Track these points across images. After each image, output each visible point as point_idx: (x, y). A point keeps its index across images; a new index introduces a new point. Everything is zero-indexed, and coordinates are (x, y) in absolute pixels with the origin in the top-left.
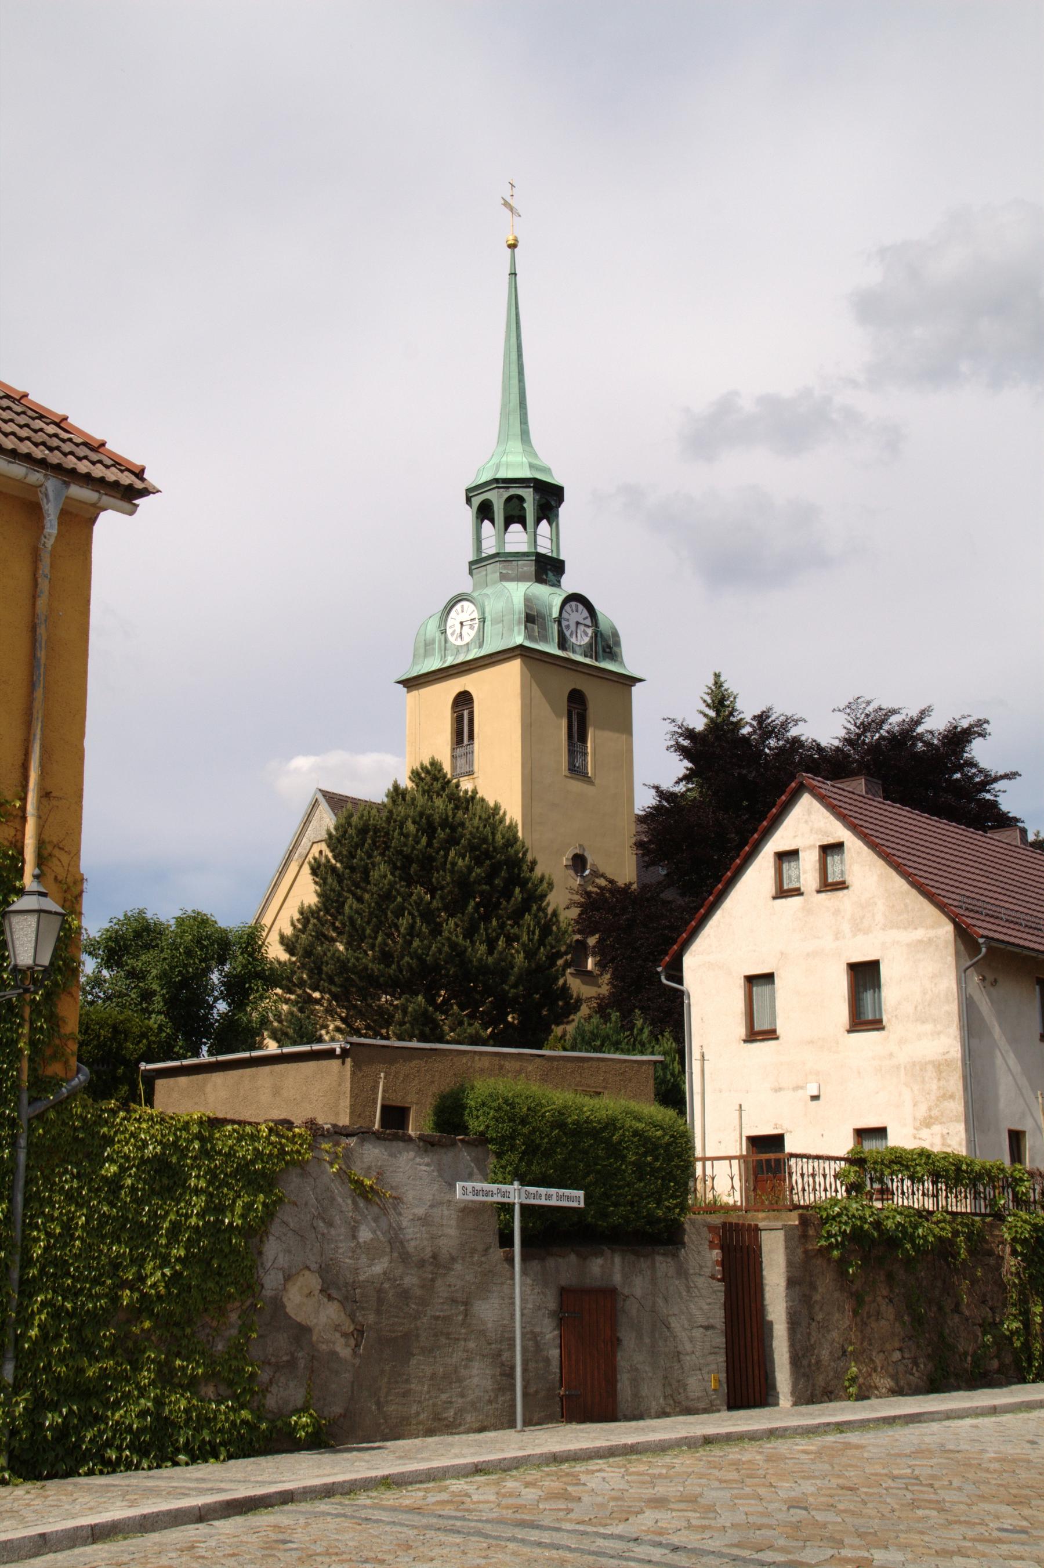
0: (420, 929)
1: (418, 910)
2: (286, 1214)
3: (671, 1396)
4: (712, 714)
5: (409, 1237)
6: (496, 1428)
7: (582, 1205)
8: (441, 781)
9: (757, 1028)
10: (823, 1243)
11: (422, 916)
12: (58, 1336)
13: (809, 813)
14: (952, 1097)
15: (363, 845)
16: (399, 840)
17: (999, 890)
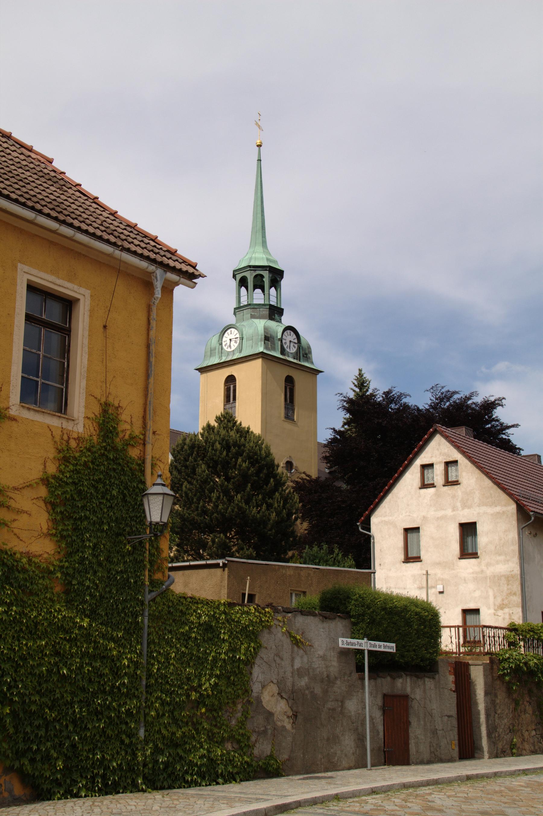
0: (223, 499)
1: (222, 490)
2: (263, 653)
3: (434, 752)
4: (357, 390)
5: (316, 666)
6: (356, 768)
7: (395, 651)
8: (232, 422)
9: (410, 556)
10: (501, 673)
12: (164, 715)
13: (439, 445)
14: (515, 594)
15: (192, 455)
16: (212, 452)
17: (534, 487)
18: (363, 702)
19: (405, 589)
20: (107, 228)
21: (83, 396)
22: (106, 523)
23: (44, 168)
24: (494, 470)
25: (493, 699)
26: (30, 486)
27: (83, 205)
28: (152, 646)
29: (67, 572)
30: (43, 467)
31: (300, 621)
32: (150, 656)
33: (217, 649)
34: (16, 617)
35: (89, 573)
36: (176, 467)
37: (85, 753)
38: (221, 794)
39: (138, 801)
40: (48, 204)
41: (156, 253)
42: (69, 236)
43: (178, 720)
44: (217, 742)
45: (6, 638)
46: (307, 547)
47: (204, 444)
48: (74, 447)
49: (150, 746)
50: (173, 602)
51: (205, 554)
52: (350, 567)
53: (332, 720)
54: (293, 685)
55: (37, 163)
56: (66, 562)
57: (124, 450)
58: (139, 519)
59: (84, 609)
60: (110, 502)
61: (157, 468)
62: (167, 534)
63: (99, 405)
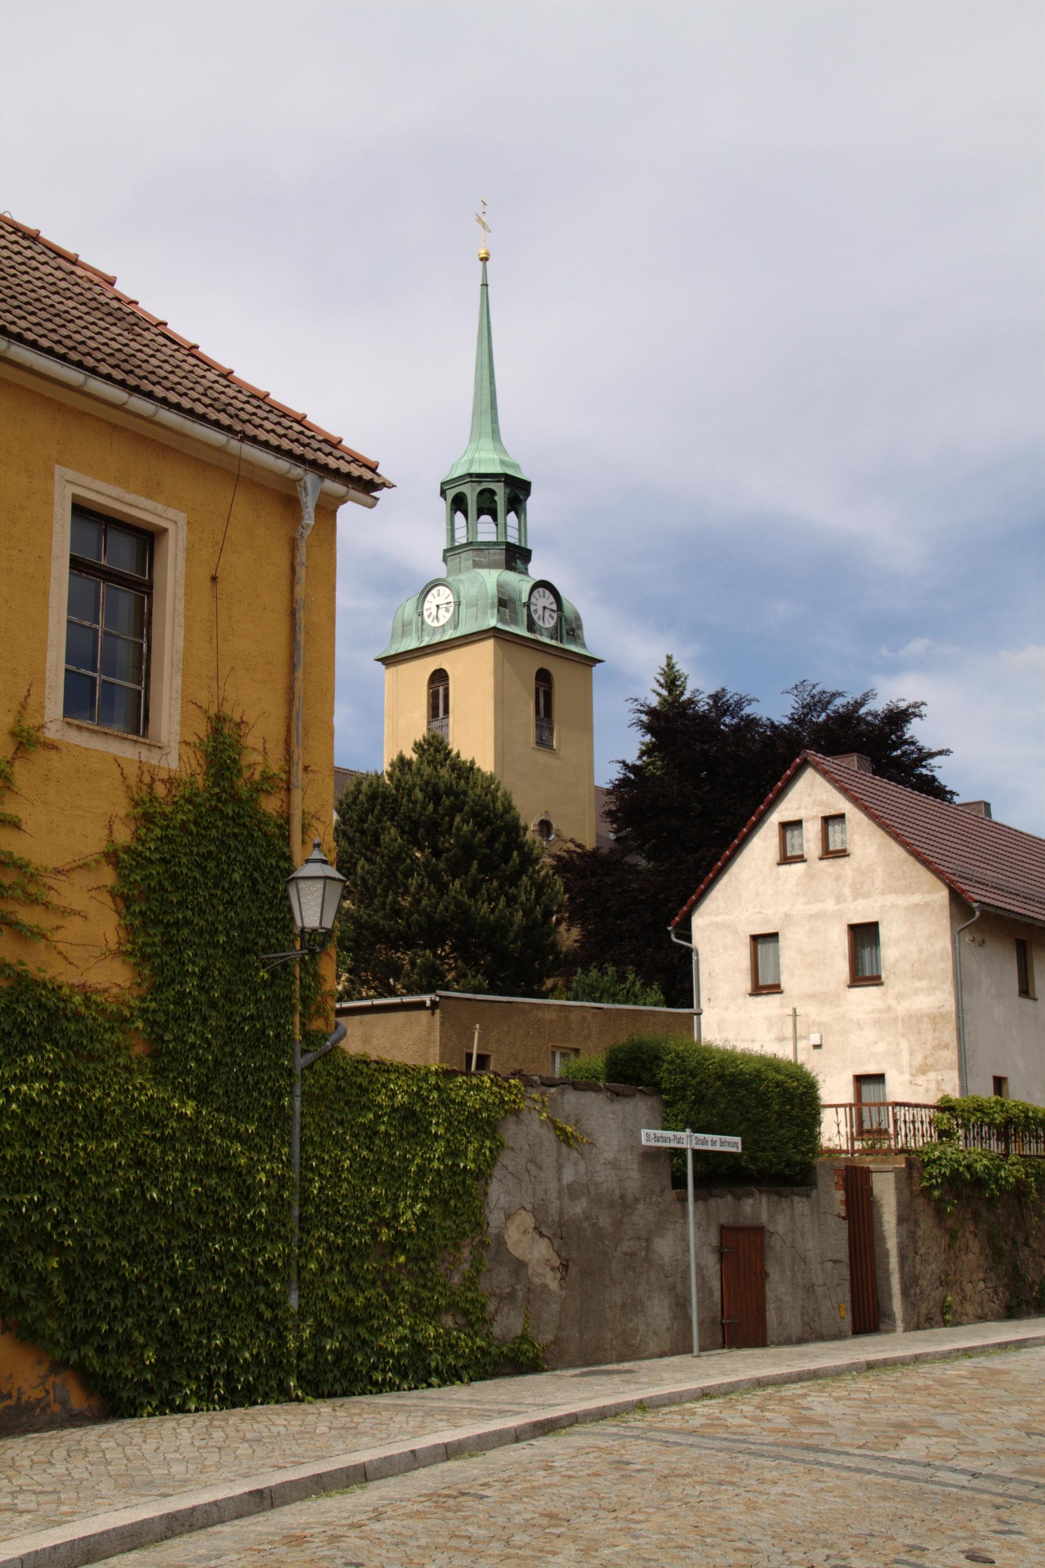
0: (428, 888)
2: (506, 1158)
3: (808, 1323)
4: (665, 693)
5: (601, 1180)
6: (673, 1354)
7: (740, 1150)
8: (442, 752)
9: (761, 983)
10: (925, 1184)
11: (429, 877)
12: (332, 1268)
13: (812, 787)
14: (946, 1046)
15: (373, 811)
18: (685, 1239)
19: (753, 1041)
20: (215, 400)
21: (177, 705)
22: (221, 932)
23: (100, 294)
24: (909, 829)
25: (913, 1229)
26: (84, 866)
27: (170, 360)
28: (310, 1149)
29: (155, 1020)
30: (107, 831)
31: (572, 1099)
32: (306, 1166)
33: (425, 1153)
34: (65, 1100)
35: (193, 1020)
36: (345, 834)
37: (194, 1337)
38: (435, 1404)
39: (289, 1417)
40: (107, 358)
41: (304, 445)
42: (146, 415)
43: (356, 1277)
44: (427, 1315)
45: (49, 1136)
46: (579, 970)
47: (394, 792)
48: (163, 795)
49: (309, 1323)
50: (344, 1070)
51: (399, 986)
52: (655, 1005)
53: (630, 1273)
54: (561, 1214)
55: (87, 285)
56: (151, 1000)
57: (251, 799)
58: (282, 923)
59: (187, 1085)
60: (229, 894)
61: (312, 833)
62: (332, 949)
63: (206, 719)
